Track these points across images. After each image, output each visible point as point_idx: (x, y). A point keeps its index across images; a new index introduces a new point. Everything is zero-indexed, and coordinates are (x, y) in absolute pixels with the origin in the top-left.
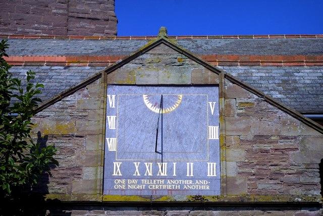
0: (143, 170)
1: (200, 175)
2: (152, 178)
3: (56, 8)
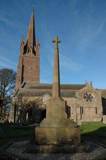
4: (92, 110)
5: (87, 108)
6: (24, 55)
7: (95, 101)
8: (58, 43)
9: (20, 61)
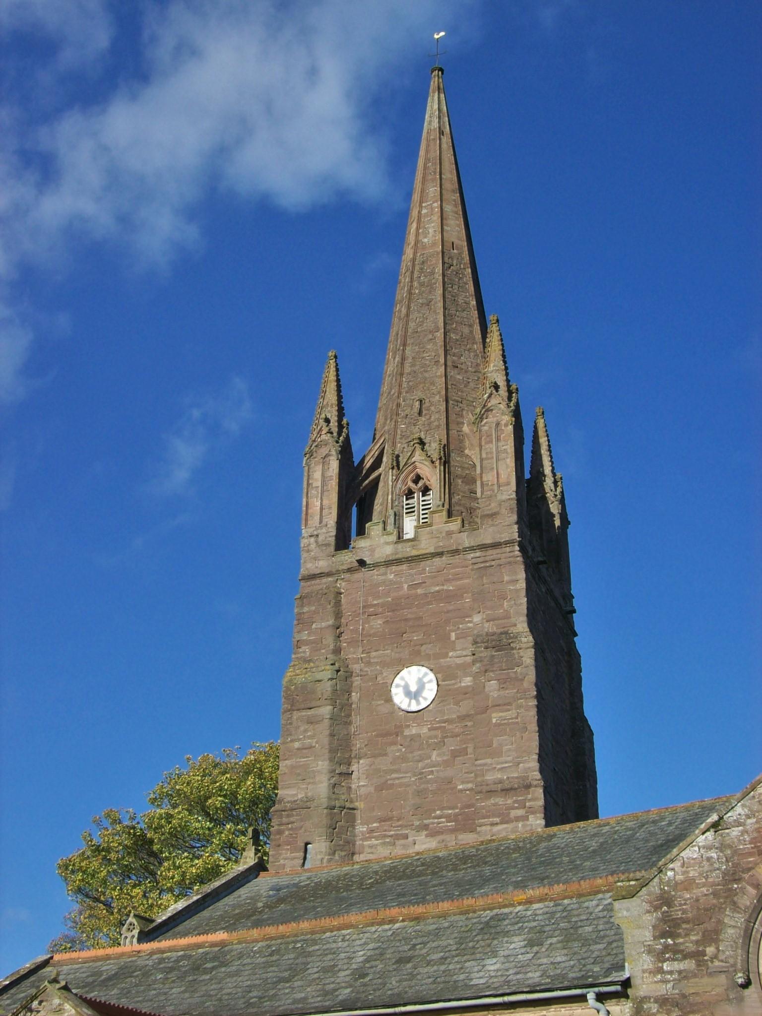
3: (463, 783)
6: (347, 558)
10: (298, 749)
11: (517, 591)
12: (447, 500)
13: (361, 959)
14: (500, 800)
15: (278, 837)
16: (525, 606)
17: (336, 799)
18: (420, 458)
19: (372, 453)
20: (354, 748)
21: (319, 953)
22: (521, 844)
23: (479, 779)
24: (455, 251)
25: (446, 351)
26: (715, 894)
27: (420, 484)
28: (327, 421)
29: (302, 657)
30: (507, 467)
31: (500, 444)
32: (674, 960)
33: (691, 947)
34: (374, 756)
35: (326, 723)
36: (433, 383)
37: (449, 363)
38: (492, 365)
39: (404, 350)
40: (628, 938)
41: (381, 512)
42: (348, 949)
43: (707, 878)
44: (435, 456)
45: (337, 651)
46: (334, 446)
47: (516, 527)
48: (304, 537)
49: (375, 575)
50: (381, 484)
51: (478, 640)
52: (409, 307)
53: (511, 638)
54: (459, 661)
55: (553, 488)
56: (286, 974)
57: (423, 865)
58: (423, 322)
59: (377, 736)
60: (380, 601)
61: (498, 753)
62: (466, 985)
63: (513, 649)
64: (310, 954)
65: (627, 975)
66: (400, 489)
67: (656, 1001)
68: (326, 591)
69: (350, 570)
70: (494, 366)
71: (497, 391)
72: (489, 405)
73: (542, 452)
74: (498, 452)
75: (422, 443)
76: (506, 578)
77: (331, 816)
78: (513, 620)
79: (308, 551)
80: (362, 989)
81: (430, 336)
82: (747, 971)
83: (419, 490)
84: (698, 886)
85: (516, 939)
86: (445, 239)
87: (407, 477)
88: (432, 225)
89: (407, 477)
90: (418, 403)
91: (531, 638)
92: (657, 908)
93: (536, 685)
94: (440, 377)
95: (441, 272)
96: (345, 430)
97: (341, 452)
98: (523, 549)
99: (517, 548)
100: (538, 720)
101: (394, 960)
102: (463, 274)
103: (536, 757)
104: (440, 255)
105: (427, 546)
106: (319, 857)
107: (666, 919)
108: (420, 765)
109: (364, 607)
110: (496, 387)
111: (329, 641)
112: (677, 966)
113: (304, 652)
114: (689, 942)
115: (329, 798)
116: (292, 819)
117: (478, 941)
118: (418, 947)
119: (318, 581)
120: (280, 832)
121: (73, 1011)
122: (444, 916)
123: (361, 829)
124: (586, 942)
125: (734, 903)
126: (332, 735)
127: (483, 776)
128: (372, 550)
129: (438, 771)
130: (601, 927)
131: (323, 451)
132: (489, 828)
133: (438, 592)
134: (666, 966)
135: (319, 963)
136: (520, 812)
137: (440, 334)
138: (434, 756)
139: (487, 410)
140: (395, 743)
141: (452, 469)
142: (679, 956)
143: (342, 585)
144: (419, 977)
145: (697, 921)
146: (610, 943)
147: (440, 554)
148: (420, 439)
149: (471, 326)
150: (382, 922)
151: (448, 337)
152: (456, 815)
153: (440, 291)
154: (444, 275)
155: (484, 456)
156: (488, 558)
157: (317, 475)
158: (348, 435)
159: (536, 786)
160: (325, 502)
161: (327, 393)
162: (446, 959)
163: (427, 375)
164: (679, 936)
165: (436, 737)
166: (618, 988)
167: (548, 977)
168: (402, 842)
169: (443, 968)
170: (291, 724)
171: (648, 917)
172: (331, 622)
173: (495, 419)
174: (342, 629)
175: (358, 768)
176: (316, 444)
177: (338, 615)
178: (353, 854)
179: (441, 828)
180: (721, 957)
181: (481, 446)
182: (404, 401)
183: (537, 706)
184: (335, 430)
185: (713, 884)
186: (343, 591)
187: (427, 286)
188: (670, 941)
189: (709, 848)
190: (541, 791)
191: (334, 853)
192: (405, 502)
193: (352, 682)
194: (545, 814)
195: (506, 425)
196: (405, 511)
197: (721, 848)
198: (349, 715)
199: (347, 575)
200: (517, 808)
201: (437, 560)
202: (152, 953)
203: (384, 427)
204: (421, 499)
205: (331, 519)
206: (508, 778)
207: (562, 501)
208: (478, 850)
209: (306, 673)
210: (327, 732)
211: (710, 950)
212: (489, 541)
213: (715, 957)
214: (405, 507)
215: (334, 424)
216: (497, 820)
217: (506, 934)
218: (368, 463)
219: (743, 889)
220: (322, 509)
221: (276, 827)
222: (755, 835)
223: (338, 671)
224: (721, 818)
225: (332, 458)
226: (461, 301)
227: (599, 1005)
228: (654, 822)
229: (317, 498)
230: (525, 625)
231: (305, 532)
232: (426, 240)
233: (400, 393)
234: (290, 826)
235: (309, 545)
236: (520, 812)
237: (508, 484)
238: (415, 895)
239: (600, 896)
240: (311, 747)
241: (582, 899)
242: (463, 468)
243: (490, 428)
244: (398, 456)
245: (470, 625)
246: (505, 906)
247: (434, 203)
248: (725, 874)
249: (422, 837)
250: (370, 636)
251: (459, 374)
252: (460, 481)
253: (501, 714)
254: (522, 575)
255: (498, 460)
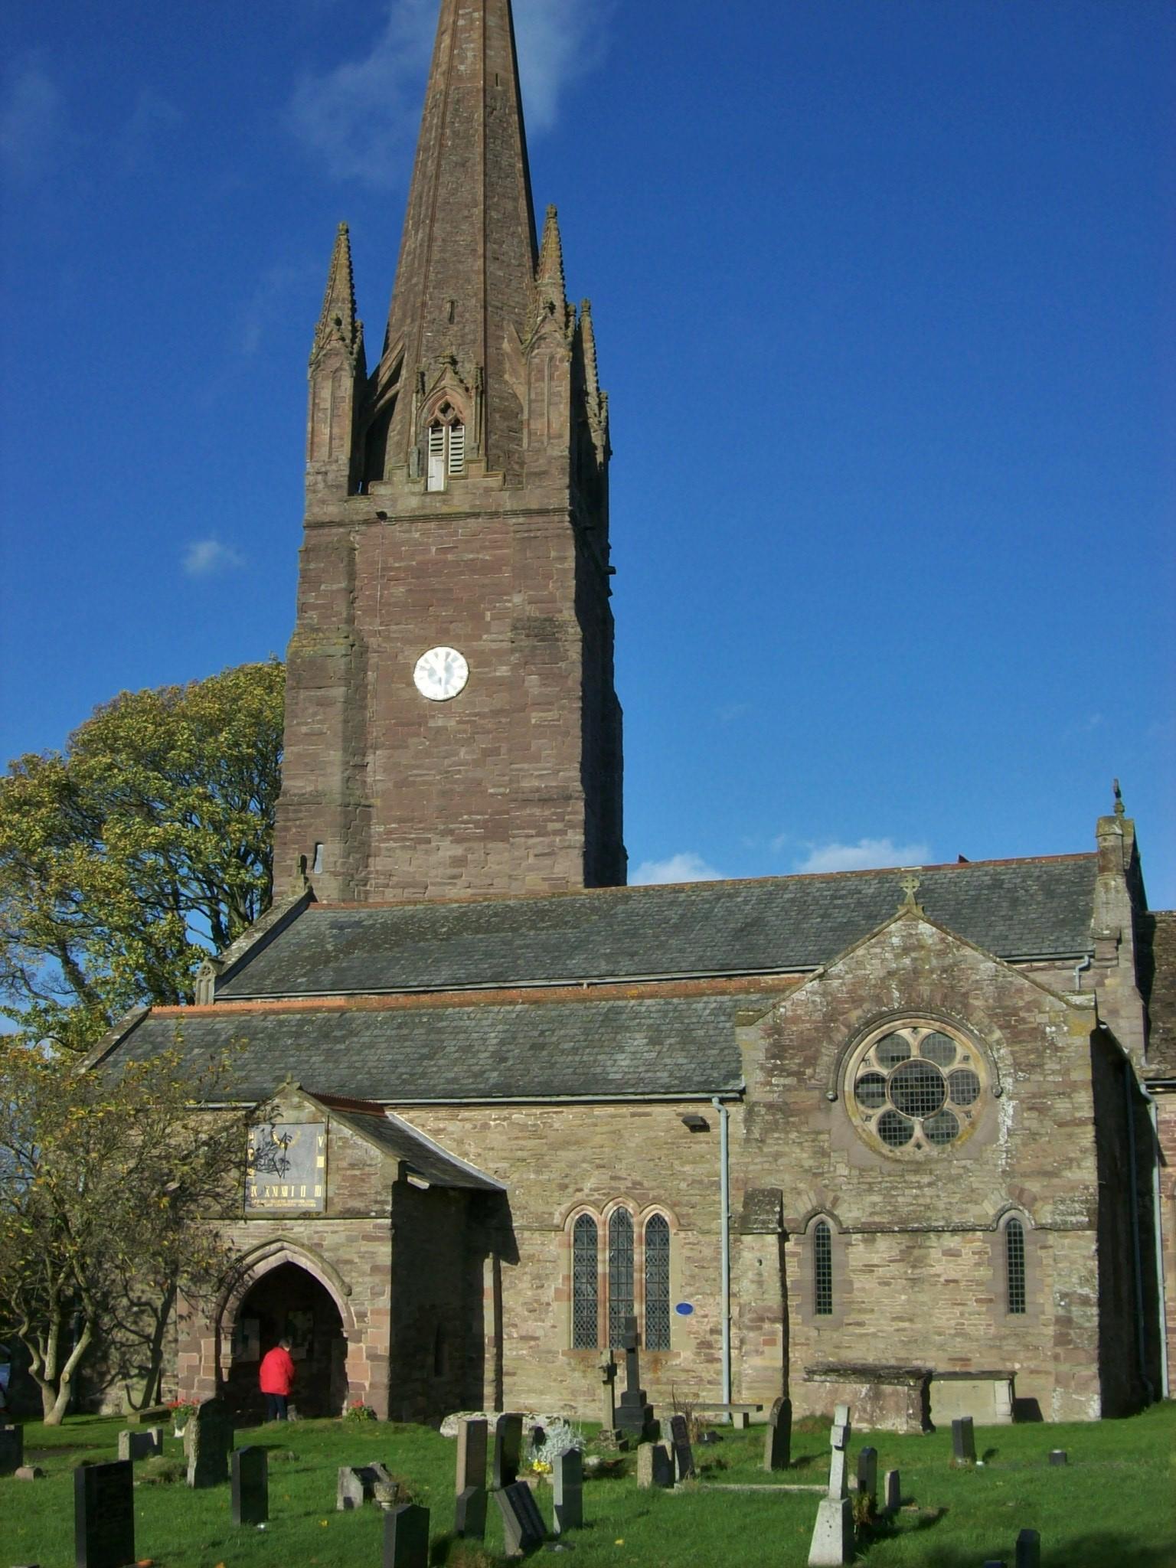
0: (271, 1192)
1: (310, 1195)
2: (278, 1198)
3: (494, 786)
4: (940, 1266)
5: (883, 1243)
6: (362, 506)
7: (994, 1138)
8: (429, 490)
9: (311, 598)
10: (306, 734)
11: (565, 571)
12: (483, 442)
13: (495, 1041)
14: (537, 811)
15: (283, 834)
16: (573, 590)
17: (350, 795)
18: (450, 382)
19: (389, 364)
20: (370, 737)
21: (449, 1030)
22: (597, 903)
23: (515, 786)
24: (499, 88)
25: (485, 236)
26: (816, 1029)
27: (450, 415)
28: (338, 322)
29: (307, 625)
30: (561, 415)
31: (554, 384)
32: (781, 1076)
33: (795, 1068)
34: (393, 747)
35: (339, 706)
36: (468, 281)
37: (489, 254)
38: (547, 276)
39: (431, 227)
40: (745, 1058)
41: (399, 444)
42: (477, 1029)
43: (810, 1016)
44: (470, 383)
45: (350, 620)
46: (348, 359)
47: (567, 491)
48: (308, 474)
49: (396, 531)
50: (398, 406)
51: (518, 625)
52: (439, 165)
53: (556, 627)
54: (494, 646)
55: (597, 412)
56: (425, 1051)
57: (496, 915)
58: (456, 189)
59: (396, 725)
60: (402, 564)
61: (536, 758)
62: (605, 1079)
63: (557, 640)
64: (440, 1031)
65: (743, 1085)
66: (426, 419)
67: (764, 1106)
68: (337, 545)
69: (366, 522)
70: (549, 278)
71: (552, 313)
72: (543, 331)
73: (586, 361)
74: (550, 394)
75: (454, 362)
76: (553, 554)
77: (346, 814)
78: (559, 605)
79: (315, 492)
80: (508, 1074)
81: (466, 213)
82: (836, 1089)
83: (449, 423)
84: (803, 1022)
85: (637, 1035)
86: (488, 70)
87: (434, 404)
88: (472, 45)
89: (434, 404)
90: (448, 305)
91: (579, 629)
92: (769, 1036)
93: (582, 684)
94: (477, 272)
95: (482, 120)
96: (358, 334)
97: (356, 368)
98: (573, 520)
99: (567, 518)
100: (582, 725)
101: (528, 1046)
102: (508, 122)
103: (578, 766)
104: (482, 94)
105: (460, 502)
106: (332, 859)
107: (776, 1044)
108: (447, 762)
109: (383, 569)
110: (552, 308)
111: (341, 608)
112: (782, 1081)
113: (311, 618)
114: (793, 1064)
115: (343, 794)
116: (301, 815)
117: (603, 1034)
118: (547, 1033)
119: (326, 531)
120: (286, 829)
121: (313, 1108)
122: (562, 1002)
123: (377, 829)
124: (701, 1048)
125: (830, 1038)
126: (346, 721)
127: (519, 782)
128: (394, 500)
129: (466, 771)
130: (711, 1032)
131: (334, 363)
132: (523, 840)
133: (472, 560)
134: (774, 1081)
135: (455, 1042)
136: (558, 826)
137: (478, 211)
138: (463, 753)
139: (540, 338)
140: (418, 735)
141: (489, 400)
142: (785, 1074)
143: (356, 538)
144: (558, 1066)
145: (801, 1048)
146: (722, 1050)
147: (476, 515)
148: (452, 357)
149: (515, 199)
150: (502, 1003)
151: (488, 216)
152: (486, 821)
153: (480, 149)
154: (485, 126)
155: (533, 396)
156: (533, 527)
157: (326, 393)
158: (362, 342)
159: (577, 799)
160: (336, 430)
161: (337, 282)
162: (578, 1049)
163: (461, 267)
164: (785, 1058)
165: (465, 731)
166: (738, 1095)
167: (676, 1078)
168: (423, 846)
169: (577, 1058)
170: (296, 704)
171: (762, 1042)
172: (343, 585)
173: (548, 350)
174: (356, 594)
175: (375, 760)
176: (324, 352)
177: (352, 576)
178: (369, 856)
179: (468, 834)
180: (817, 1077)
181: (529, 383)
182: (431, 299)
183: (582, 709)
184: (348, 335)
185: (816, 1022)
186: (357, 546)
187: (464, 138)
188: (778, 1062)
189: (814, 993)
190: (582, 804)
191: (348, 857)
192: (431, 436)
193: (368, 659)
194: (585, 829)
195: (562, 360)
196: (430, 448)
197: (824, 994)
198: (365, 698)
199: (363, 528)
200: (553, 821)
201: (471, 521)
202: (266, 1014)
203: (402, 325)
204: (451, 434)
205: (344, 453)
206: (546, 787)
207: (606, 431)
208: (551, 903)
209: (315, 645)
210: (341, 718)
211: (809, 1071)
212: (534, 506)
213: (812, 1077)
214: (431, 442)
215: (346, 326)
216: (533, 832)
217: (627, 1029)
218: (384, 377)
219: (838, 1029)
220: (331, 438)
221: (282, 823)
222: (851, 987)
223: (352, 646)
224: (826, 971)
225: (343, 373)
226: (504, 163)
227: (721, 1106)
228: (729, 896)
229: (325, 423)
230: (573, 612)
231: (309, 467)
232: (462, 68)
233: (426, 287)
234: (298, 823)
235: (316, 483)
236: (558, 826)
237: (560, 436)
238: (504, 957)
239: (705, 999)
240: (321, 733)
241: (691, 1000)
242: (501, 398)
243: (542, 361)
244: (423, 375)
245: (509, 605)
246: (619, 999)
247: (474, 11)
248: (825, 1015)
249: (446, 842)
250: (389, 605)
251: (500, 269)
252: (497, 416)
253: (542, 714)
254: (571, 553)
255: (549, 404)
